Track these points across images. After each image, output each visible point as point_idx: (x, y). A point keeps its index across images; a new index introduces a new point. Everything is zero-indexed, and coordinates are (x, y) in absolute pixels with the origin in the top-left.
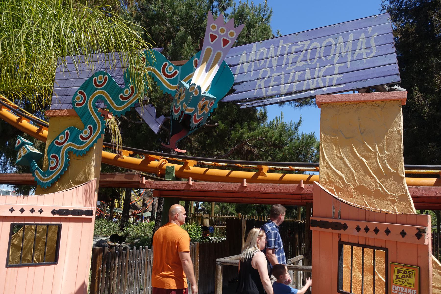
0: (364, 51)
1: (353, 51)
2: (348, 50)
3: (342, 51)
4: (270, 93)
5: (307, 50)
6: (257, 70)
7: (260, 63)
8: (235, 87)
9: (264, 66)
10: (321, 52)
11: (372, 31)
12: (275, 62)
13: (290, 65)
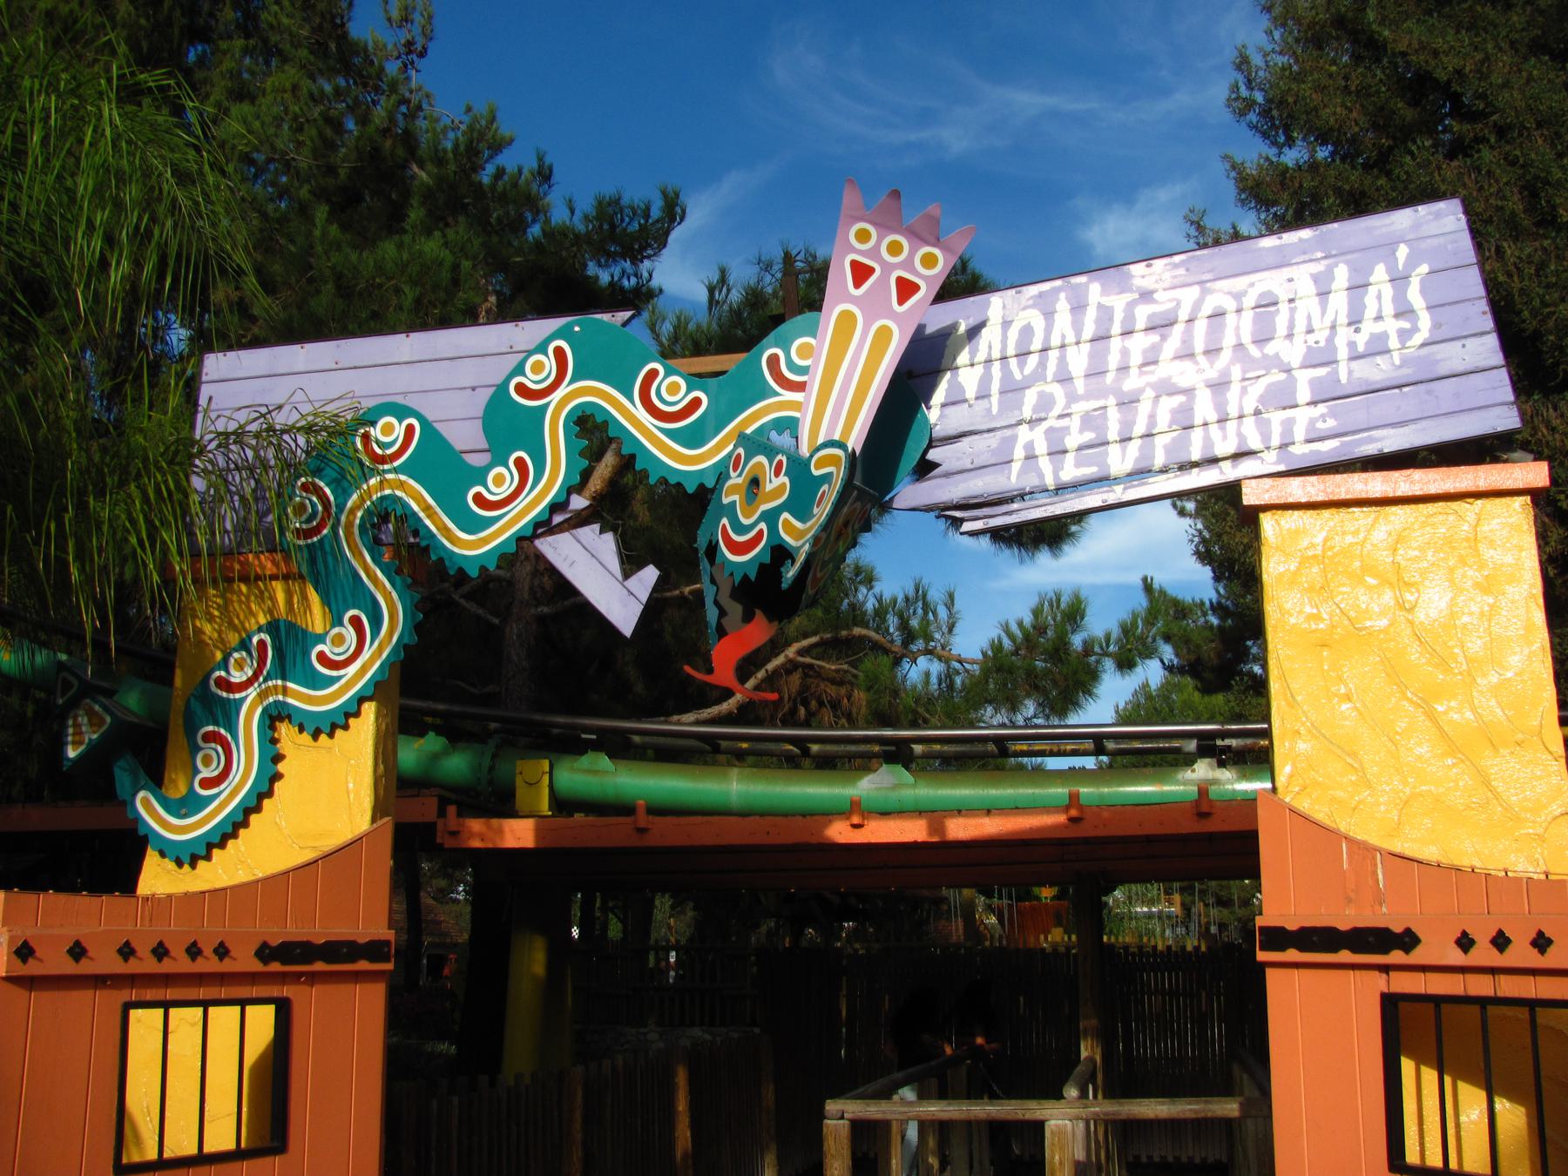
0: (1392, 326)
1: (1355, 322)
2: (1335, 320)
3: (1316, 324)
4: (1070, 472)
5: (1045, 350)
6: (1012, 390)
7: (1021, 366)
8: (933, 455)
9: (1039, 375)
10: (1240, 327)
11: (1409, 257)
12: (1078, 361)
13: (1134, 371)
